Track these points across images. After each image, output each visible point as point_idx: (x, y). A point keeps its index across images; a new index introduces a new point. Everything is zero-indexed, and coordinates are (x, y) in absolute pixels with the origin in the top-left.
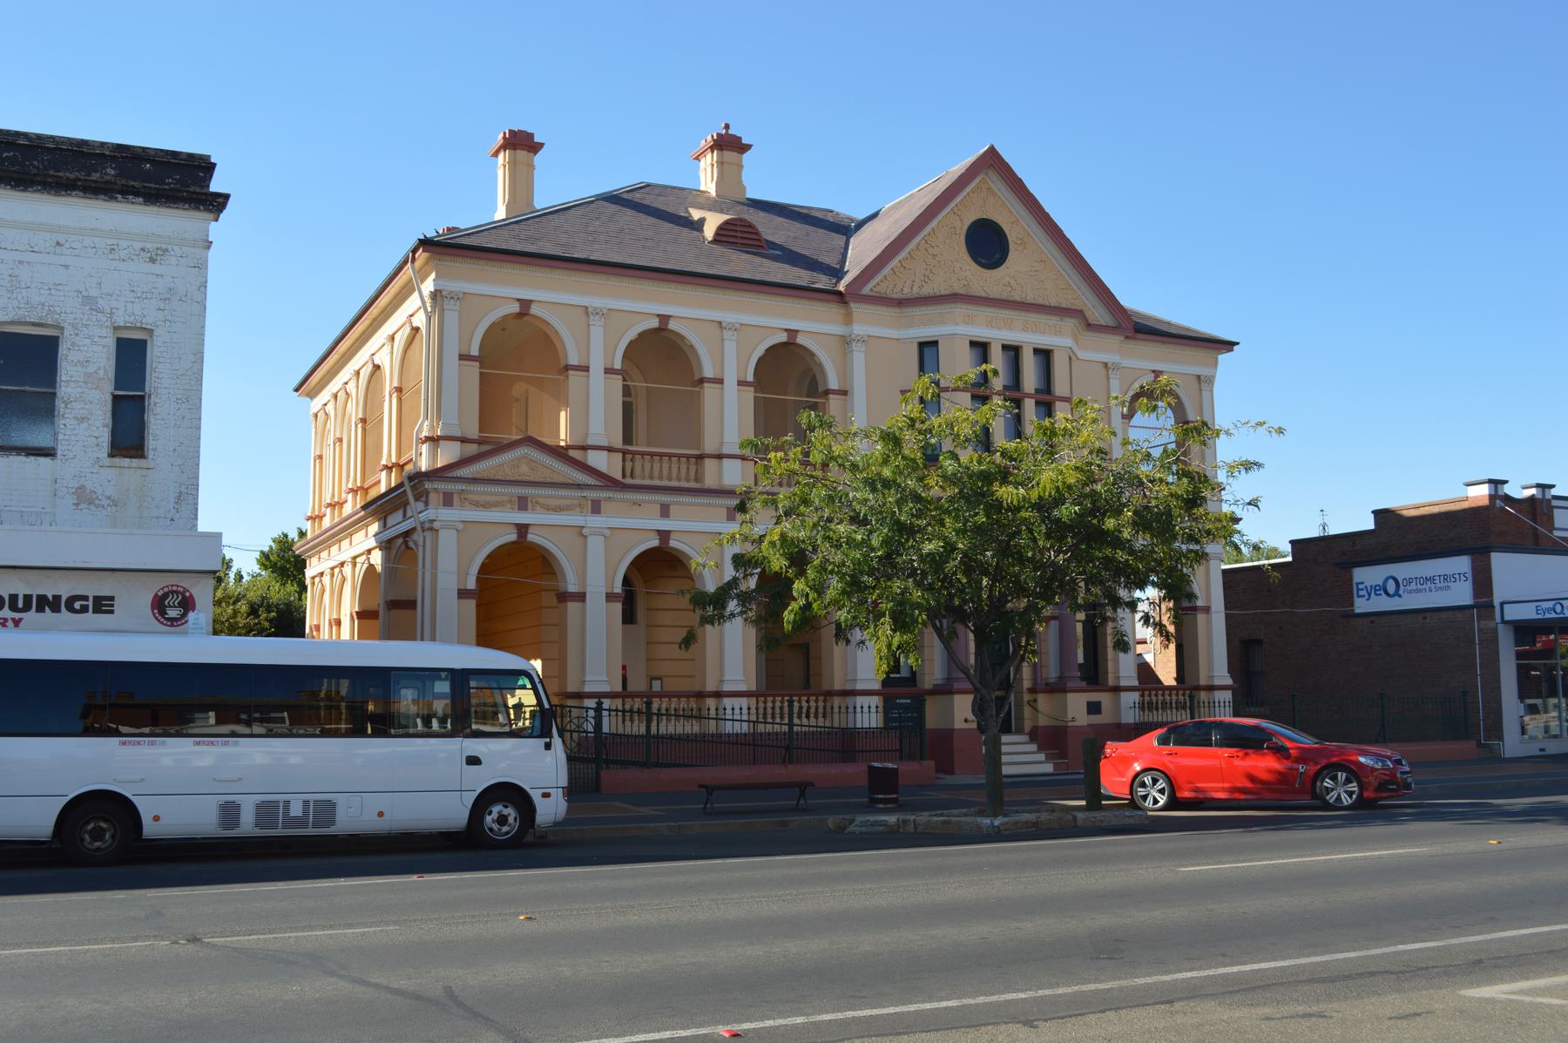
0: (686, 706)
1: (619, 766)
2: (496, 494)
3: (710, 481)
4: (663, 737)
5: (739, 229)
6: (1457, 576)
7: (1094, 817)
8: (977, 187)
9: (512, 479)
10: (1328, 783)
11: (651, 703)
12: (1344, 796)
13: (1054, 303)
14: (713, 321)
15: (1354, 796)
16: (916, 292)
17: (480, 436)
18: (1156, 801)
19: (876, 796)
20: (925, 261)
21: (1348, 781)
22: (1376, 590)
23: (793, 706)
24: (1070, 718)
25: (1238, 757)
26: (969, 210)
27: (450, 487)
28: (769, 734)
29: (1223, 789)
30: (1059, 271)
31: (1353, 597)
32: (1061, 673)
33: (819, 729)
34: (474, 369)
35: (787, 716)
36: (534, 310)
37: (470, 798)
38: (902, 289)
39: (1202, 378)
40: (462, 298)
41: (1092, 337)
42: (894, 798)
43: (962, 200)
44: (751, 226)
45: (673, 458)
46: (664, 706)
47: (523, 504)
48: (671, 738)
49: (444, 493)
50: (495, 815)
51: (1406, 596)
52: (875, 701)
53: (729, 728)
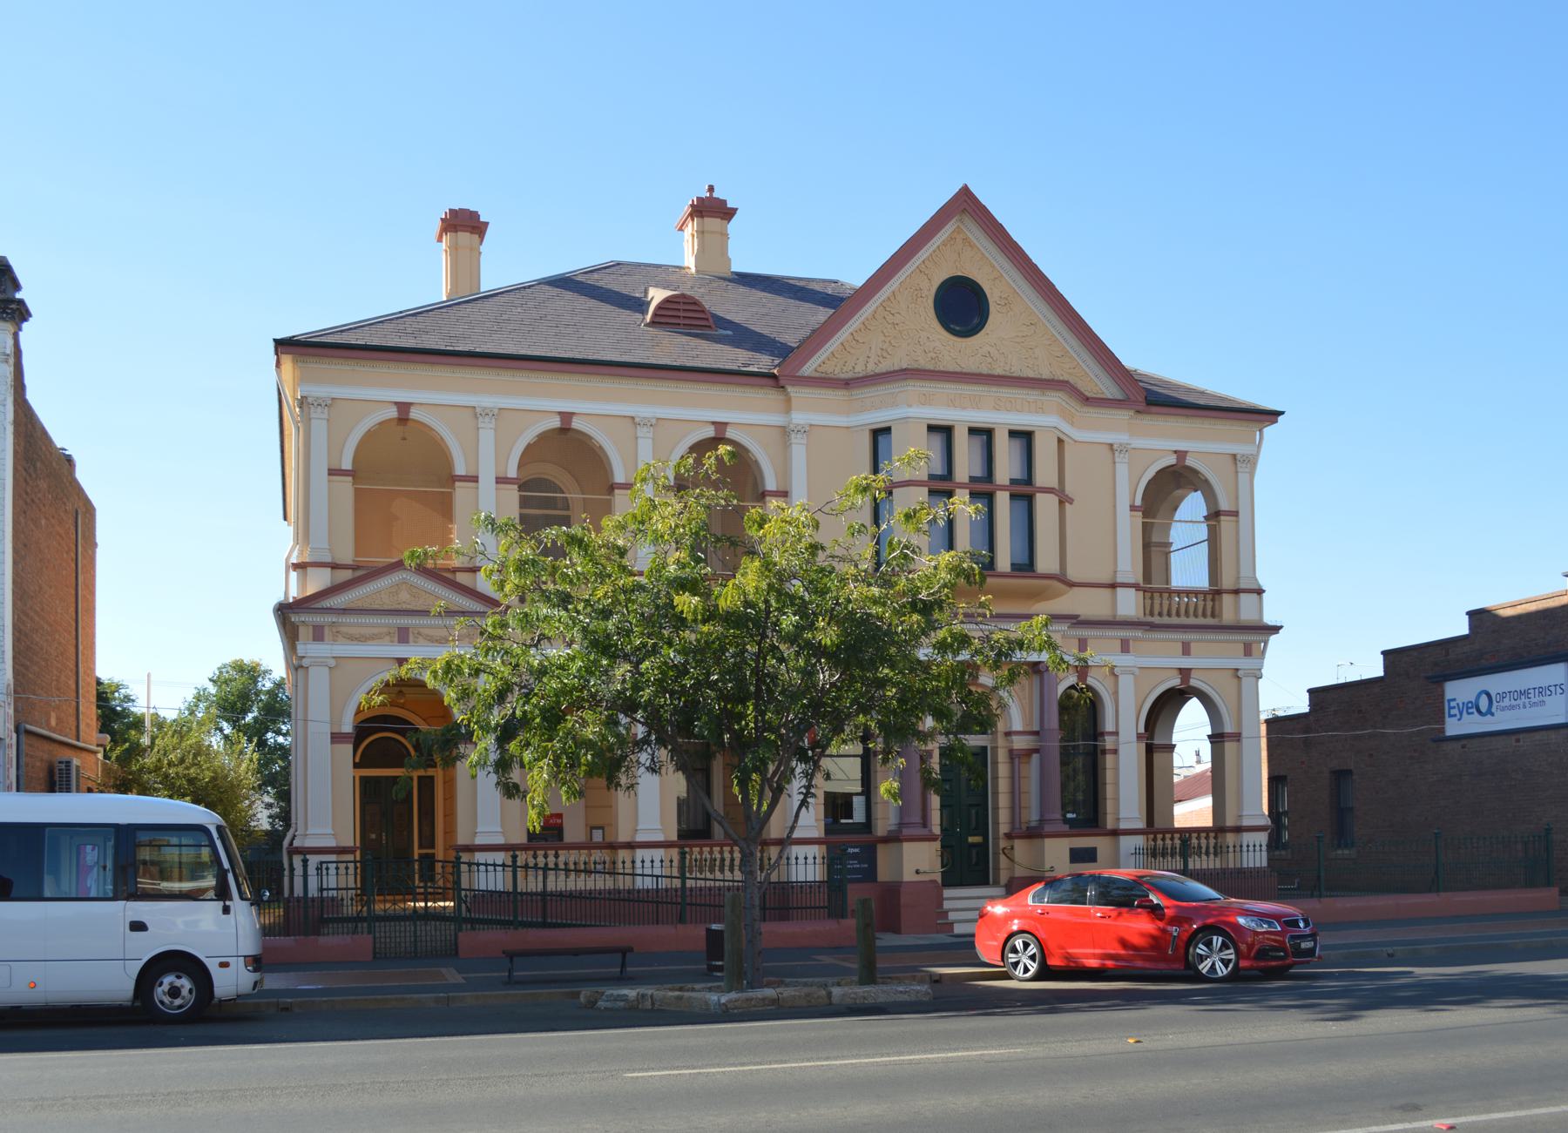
1: (498, 927)
2: (373, 626)
3: (1228, 617)
4: (552, 894)
5: (681, 307)
6: (1552, 689)
7: (855, 993)
8: (951, 239)
9: (389, 608)
10: (1201, 949)
11: (517, 856)
12: (1219, 965)
13: (1046, 375)
14: (625, 417)
15: (1231, 966)
16: (872, 368)
17: (354, 561)
18: (1026, 970)
19: (714, 963)
20: (883, 332)
21: (1224, 946)
22: (1468, 708)
23: (685, 858)
24: (1047, 867)
25: (1109, 917)
26: (938, 267)
27: (319, 619)
28: (667, 890)
29: (1094, 956)
30: (1053, 335)
31: (1444, 717)
32: (1042, 815)
33: (736, 884)
34: (346, 486)
36: (415, 414)
37: (135, 968)
38: (854, 368)
39: (1238, 457)
40: (331, 405)
41: (1093, 413)
42: (719, 966)
43: (931, 255)
44: (696, 303)
46: (572, 859)
47: (403, 636)
48: (561, 895)
49: (314, 626)
50: (166, 987)
51: (1498, 714)
52: (814, 851)
53: (640, 883)
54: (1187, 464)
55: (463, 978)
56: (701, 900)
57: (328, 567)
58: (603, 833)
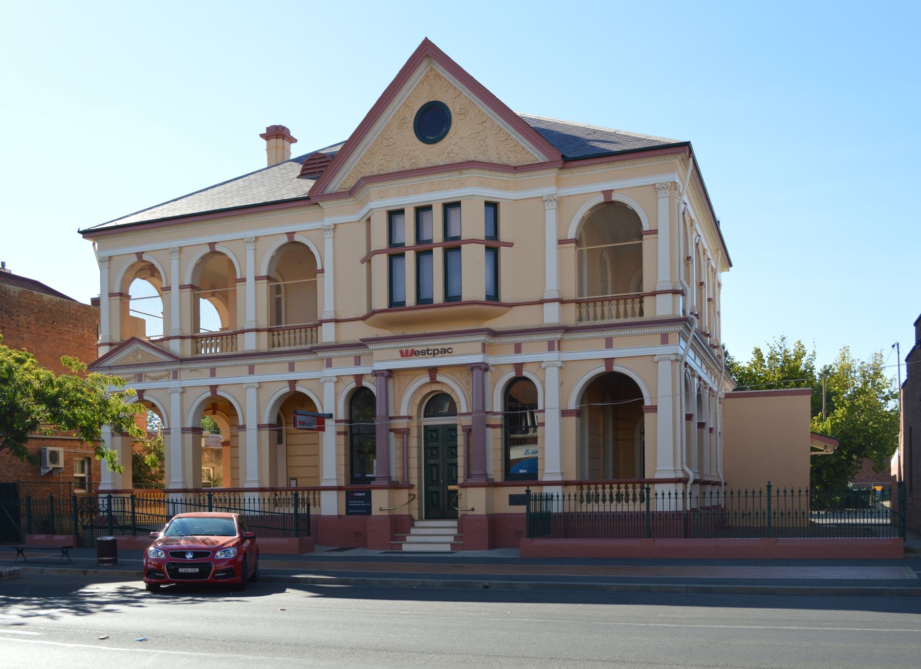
0: (285, 497)
11: (298, 494)
24: (470, 508)
28: (247, 516)
33: (276, 514)
35: (646, 500)
45: (224, 337)
47: (140, 378)
54: (612, 200)
55: (917, 574)
56: (255, 523)
57: (557, 301)
58: (296, 482)
